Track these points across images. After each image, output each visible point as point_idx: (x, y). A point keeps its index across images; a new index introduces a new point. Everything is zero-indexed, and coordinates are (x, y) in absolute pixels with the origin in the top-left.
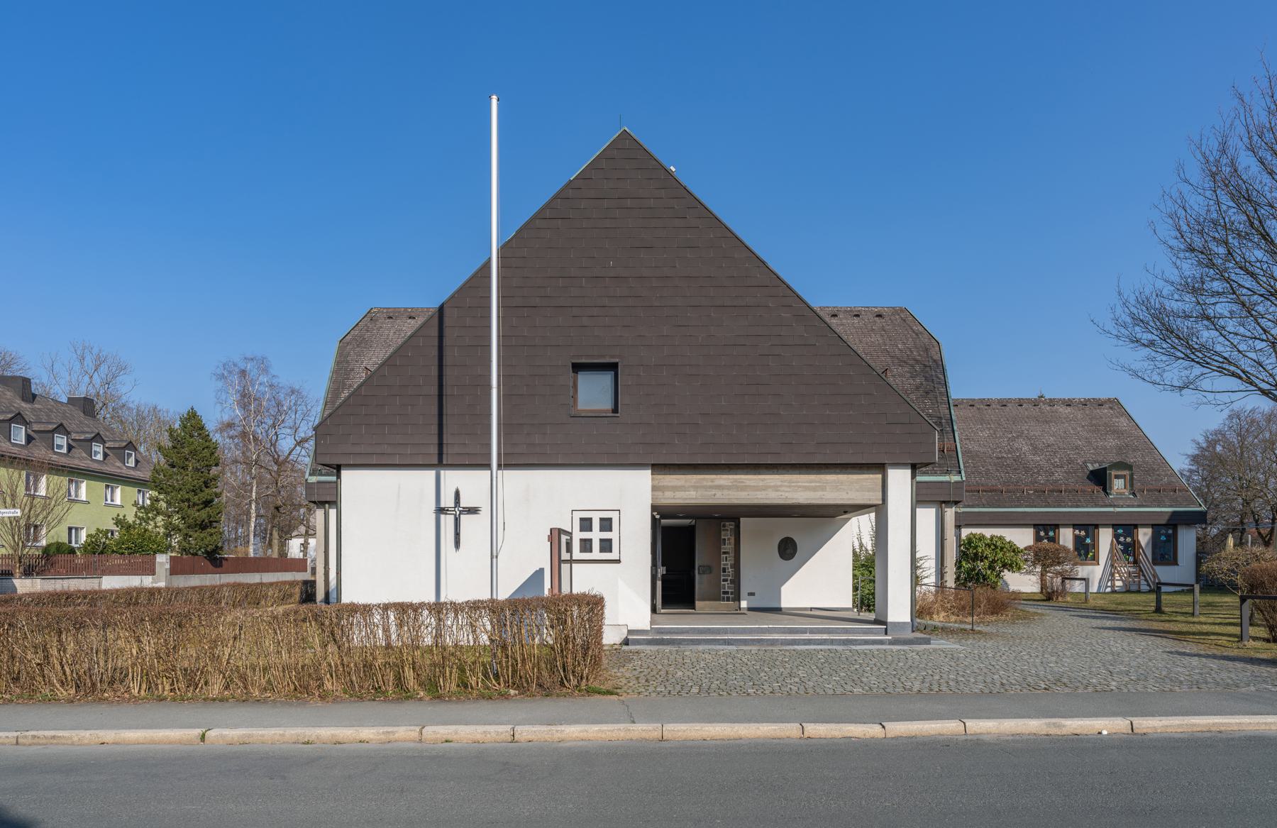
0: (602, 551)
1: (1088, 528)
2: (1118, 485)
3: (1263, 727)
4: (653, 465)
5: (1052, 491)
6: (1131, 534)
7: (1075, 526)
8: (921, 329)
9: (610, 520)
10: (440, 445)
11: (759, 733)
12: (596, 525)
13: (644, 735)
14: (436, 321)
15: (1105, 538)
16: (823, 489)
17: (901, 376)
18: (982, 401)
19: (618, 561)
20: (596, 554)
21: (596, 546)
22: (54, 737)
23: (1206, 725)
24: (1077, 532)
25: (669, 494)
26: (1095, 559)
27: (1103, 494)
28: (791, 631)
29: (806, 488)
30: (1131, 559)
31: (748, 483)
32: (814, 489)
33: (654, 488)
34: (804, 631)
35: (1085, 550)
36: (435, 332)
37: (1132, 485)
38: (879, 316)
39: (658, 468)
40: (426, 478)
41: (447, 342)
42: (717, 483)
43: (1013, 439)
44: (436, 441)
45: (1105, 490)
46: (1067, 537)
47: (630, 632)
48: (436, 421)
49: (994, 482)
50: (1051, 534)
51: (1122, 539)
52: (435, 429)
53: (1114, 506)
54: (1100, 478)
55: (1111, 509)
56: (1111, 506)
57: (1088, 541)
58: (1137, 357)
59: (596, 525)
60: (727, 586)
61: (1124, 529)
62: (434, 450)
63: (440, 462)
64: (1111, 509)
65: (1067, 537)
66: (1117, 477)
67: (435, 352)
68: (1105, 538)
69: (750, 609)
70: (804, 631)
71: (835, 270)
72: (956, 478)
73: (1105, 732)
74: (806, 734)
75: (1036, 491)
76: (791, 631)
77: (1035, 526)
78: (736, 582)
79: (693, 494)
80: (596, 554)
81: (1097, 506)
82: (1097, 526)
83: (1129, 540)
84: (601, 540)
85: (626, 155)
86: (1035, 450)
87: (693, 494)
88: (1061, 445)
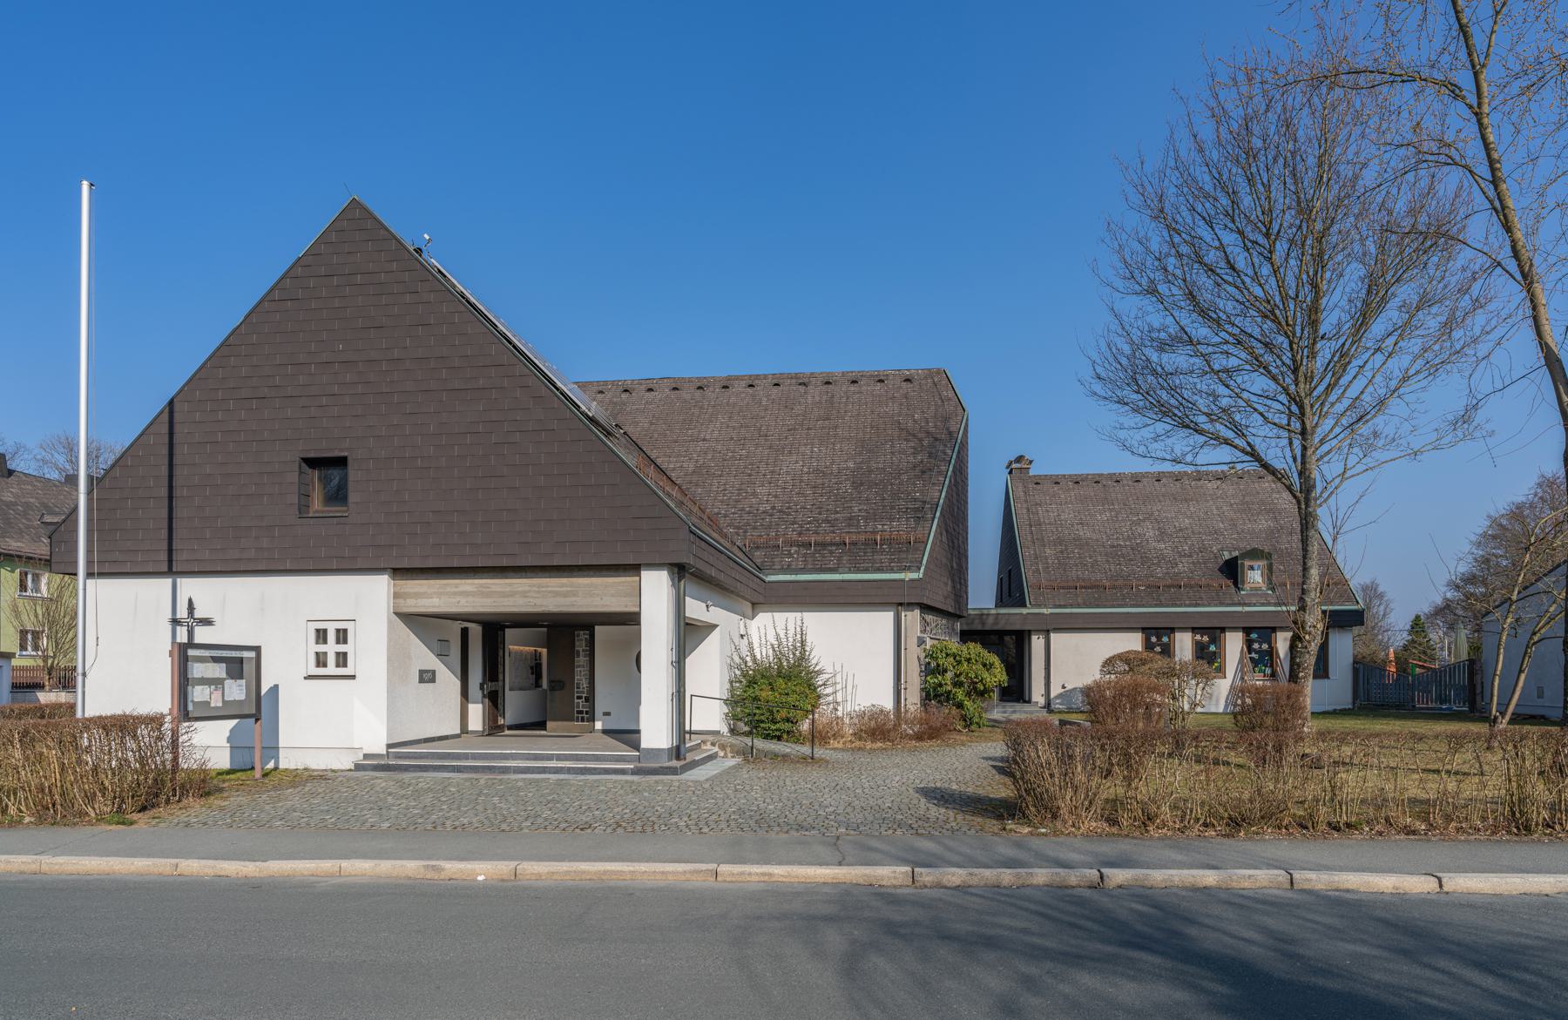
2: (1255, 577)
3: (1246, 885)
5: (1169, 587)
6: (1214, 640)
7: (1194, 630)
8: (951, 394)
9: (345, 631)
10: (170, 551)
11: (133, 868)
13: (23, 868)
14: (166, 416)
15: (1234, 644)
16: (575, 594)
18: (1111, 476)
19: (353, 677)
20: (331, 669)
21: (331, 660)
22: (742, 873)
24: (1198, 637)
25: (411, 602)
26: (1221, 671)
28: (536, 758)
30: (1268, 671)
32: (565, 595)
33: (396, 596)
34: (550, 758)
35: (1208, 656)
37: (1270, 579)
38: (907, 380)
39: (398, 572)
42: (461, 589)
43: (1138, 522)
44: (165, 546)
45: (1236, 584)
46: (1184, 645)
47: (366, 756)
48: (165, 524)
50: (1165, 639)
51: (1256, 646)
52: (164, 533)
53: (1245, 605)
54: (1231, 570)
55: (1239, 609)
56: (1239, 604)
57: (1212, 648)
60: (581, 704)
61: (1258, 634)
62: (164, 556)
63: (171, 569)
64: (1239, 609)
65: (1184, 645)
66: (1252, 568)
67: (165, 451)
68: (1234, 644)
69: (605, 732)
70: (550, 758)
71: (591, 342)
72: (914, 576)
73: (480, 878)
74: (1446, 889)
75: (1149, 586)
76: (536, 758)
77: (1143, 630)
78: (590, 699)
79: (436, 601)
81: (1222, 604)
82: (1223, 630)
83: (1265, 646)
85: (357, 225)
86: (1162, 535)
87: (463, 601)
88: (1197, 529)
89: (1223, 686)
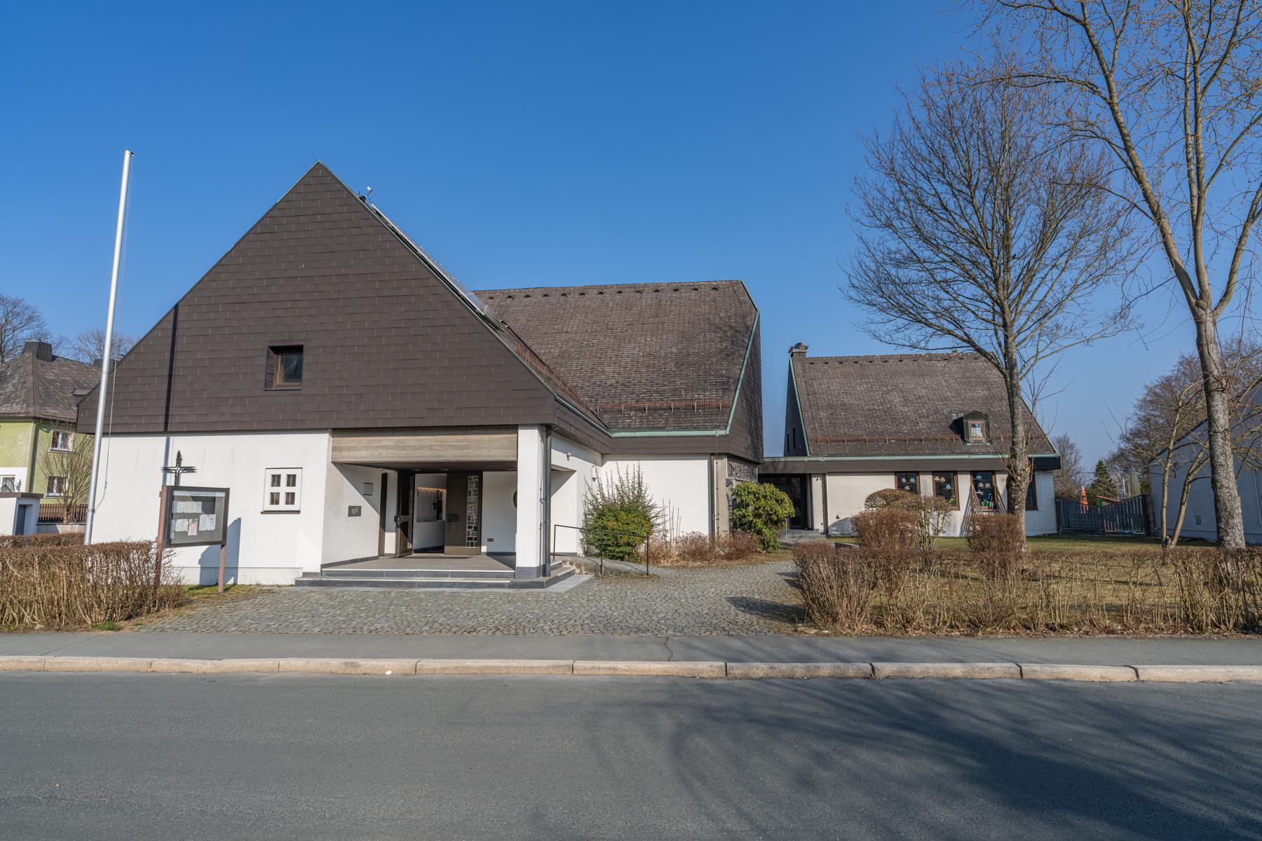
0: (287, 503)
1: (946, 476)
2: (977, 432)
4: (334, 429)
6: (949, 481)
7: (934, 473)
8: (747, 298)
10: (167, 416)
12: (284, 481)
13: (31, 666)
15: (964, 484)
17: (713, 341)
18: (866, 358)
19: (298, 512)
21: (282, 499)
22: (593, 668)
23: (479, 668)
25: (345, 454)
26: (956, 504)
27: (961, 442)
28: (436, 575)
29: (455, 447)
30: (992, 504)
31: (408, 443)
32: (462, 448)
33: (334, 449)
34: (446, 575)
35: (946, 493)
36: (170, 326)
40: (156, 444)
41: (179, 333)
42: (384, 443)
43: (888, 392)
46: (927, 484)
49: (860, 432)
50: (912, 480)
51: (981, 485)
53: (971, 453)
54: (959, 427)
55: (966, 457)
56: (966, 453)
57: (948, 487)
58: (864, 314)
59: (284, 481)
61: (982, 475)
62: (162, 420)
63: (166, 430)
64: (966, 457)
65: (927, 484)
66: (974, 426)
67: (169, 341)
68: (964, 484)
69: (489, 554)
70: (446, 575)
72: (722, 432)
73: (388, 673)
74: (1142, 678)
76: (436, 575)
77: (896, 473)
78: (478, 529)
80: (282, 506)
81: (953, 453)
82: (955, 473)
83: (988, 485)
84: (288, 494)
85: (320, 181)
86: (906, 401)
87: (384, 453)
88: (931, 397)
89: (958, 516)
